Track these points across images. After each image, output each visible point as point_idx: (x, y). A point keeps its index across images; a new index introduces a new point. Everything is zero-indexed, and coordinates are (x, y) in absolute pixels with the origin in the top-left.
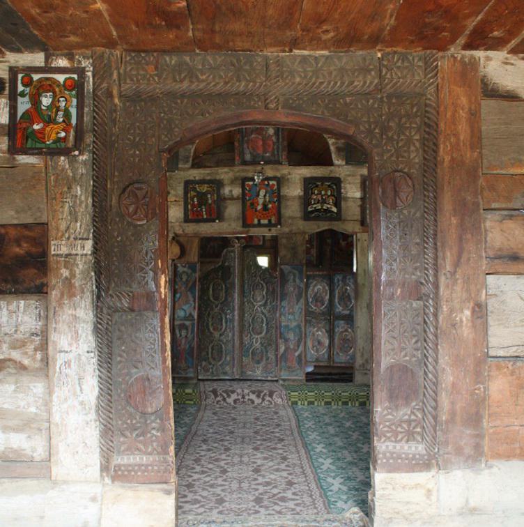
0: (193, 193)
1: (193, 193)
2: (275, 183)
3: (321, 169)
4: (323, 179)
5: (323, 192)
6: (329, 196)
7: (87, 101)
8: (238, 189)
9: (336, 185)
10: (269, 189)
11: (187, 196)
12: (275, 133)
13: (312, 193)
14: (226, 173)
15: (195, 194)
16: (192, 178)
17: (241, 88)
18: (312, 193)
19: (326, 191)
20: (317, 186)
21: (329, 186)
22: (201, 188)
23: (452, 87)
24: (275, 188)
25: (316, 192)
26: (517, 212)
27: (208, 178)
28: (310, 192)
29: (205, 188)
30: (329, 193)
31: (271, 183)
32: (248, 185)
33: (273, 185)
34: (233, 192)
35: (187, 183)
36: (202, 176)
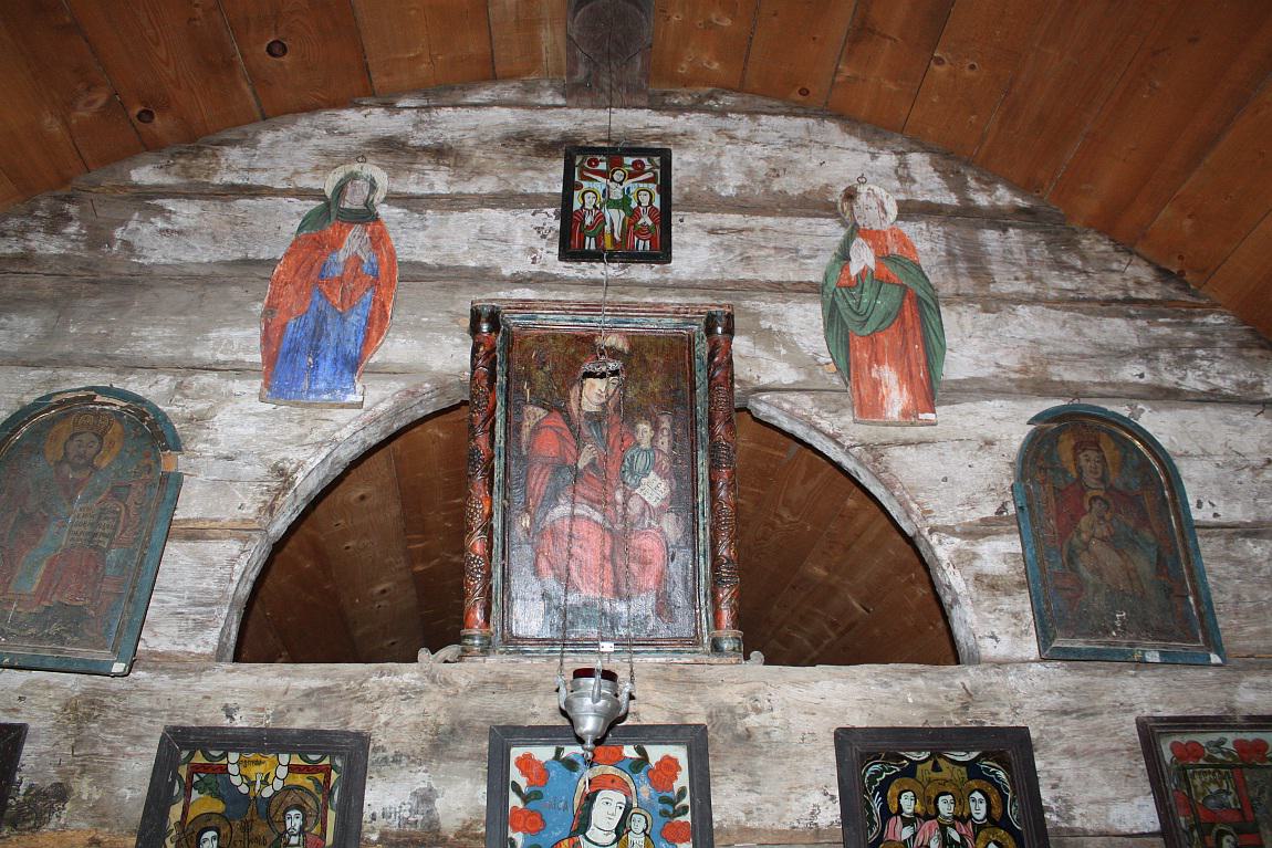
0: (202, 803)
1: (202, 803)
2: (679, 753)
3: (919, 682)
4: (938, 740)
5: (945, 807)
6: (978, 828)
7: (701, 488)
8: (467, 785)
9: (1005, 764)
10: (645, 791)
11: (165, 814)
12: (674, 498)
13: (886, 814)
14: (405, 693)
15: (219, 807)
16: (213, 717)
17: (918, 246)
18: (886, 814)
19: (961, 800)
20: (911, 771)
21: (971, 767)
22: (255, 772)
23: (296, 278)
24: (683, 780)
25: (908, 804)
26: (500, 554)
27: (302, 721)
28: (876, 805)
29: (274, 774)
30: (979, 810)
31: (656, 753)
32: (526, 764)
33: (669, 765)
34: (439, 804)
35: (179, 741)
36: (270, 706)
